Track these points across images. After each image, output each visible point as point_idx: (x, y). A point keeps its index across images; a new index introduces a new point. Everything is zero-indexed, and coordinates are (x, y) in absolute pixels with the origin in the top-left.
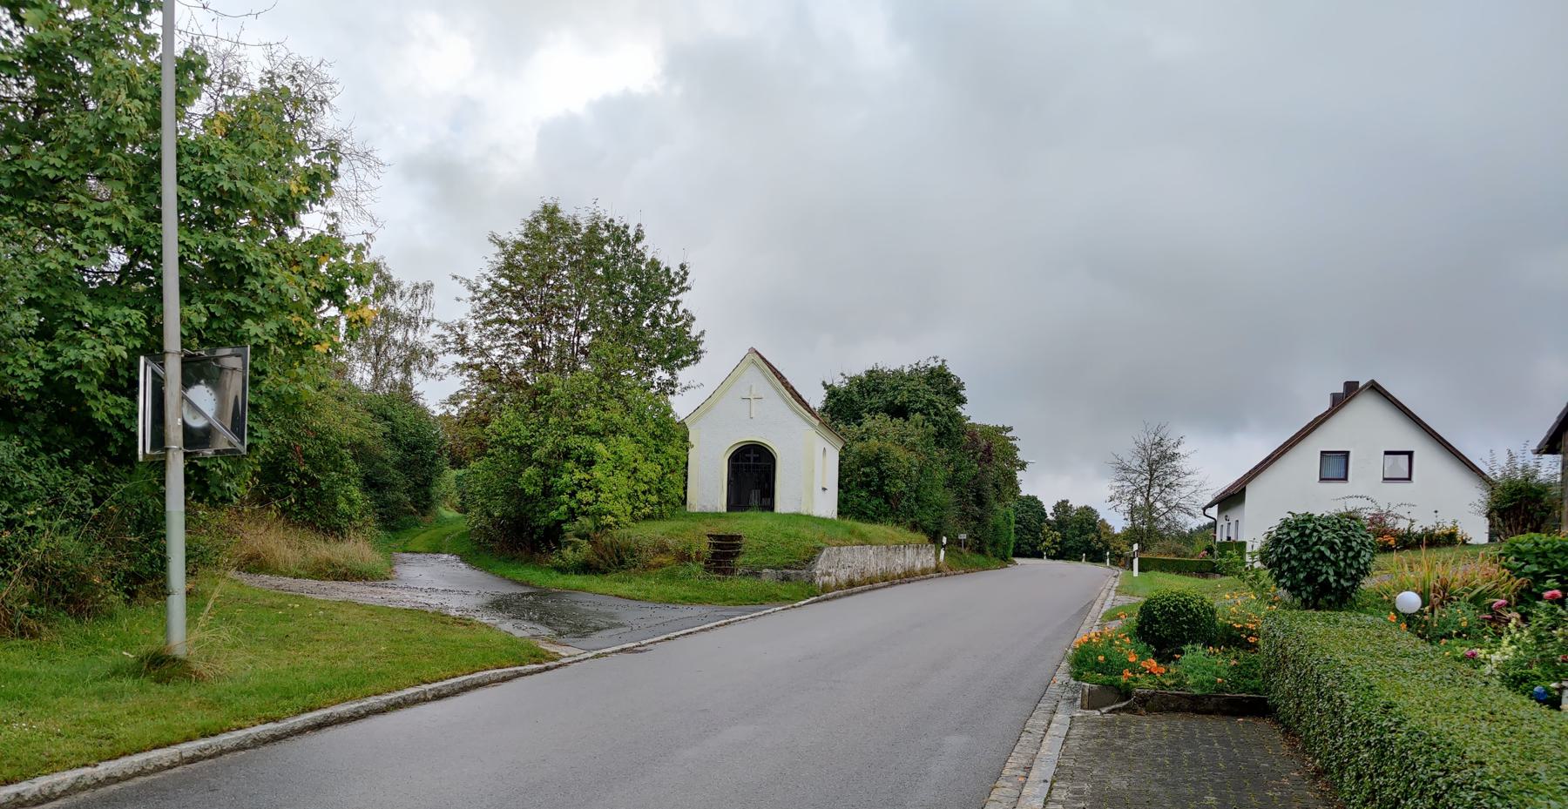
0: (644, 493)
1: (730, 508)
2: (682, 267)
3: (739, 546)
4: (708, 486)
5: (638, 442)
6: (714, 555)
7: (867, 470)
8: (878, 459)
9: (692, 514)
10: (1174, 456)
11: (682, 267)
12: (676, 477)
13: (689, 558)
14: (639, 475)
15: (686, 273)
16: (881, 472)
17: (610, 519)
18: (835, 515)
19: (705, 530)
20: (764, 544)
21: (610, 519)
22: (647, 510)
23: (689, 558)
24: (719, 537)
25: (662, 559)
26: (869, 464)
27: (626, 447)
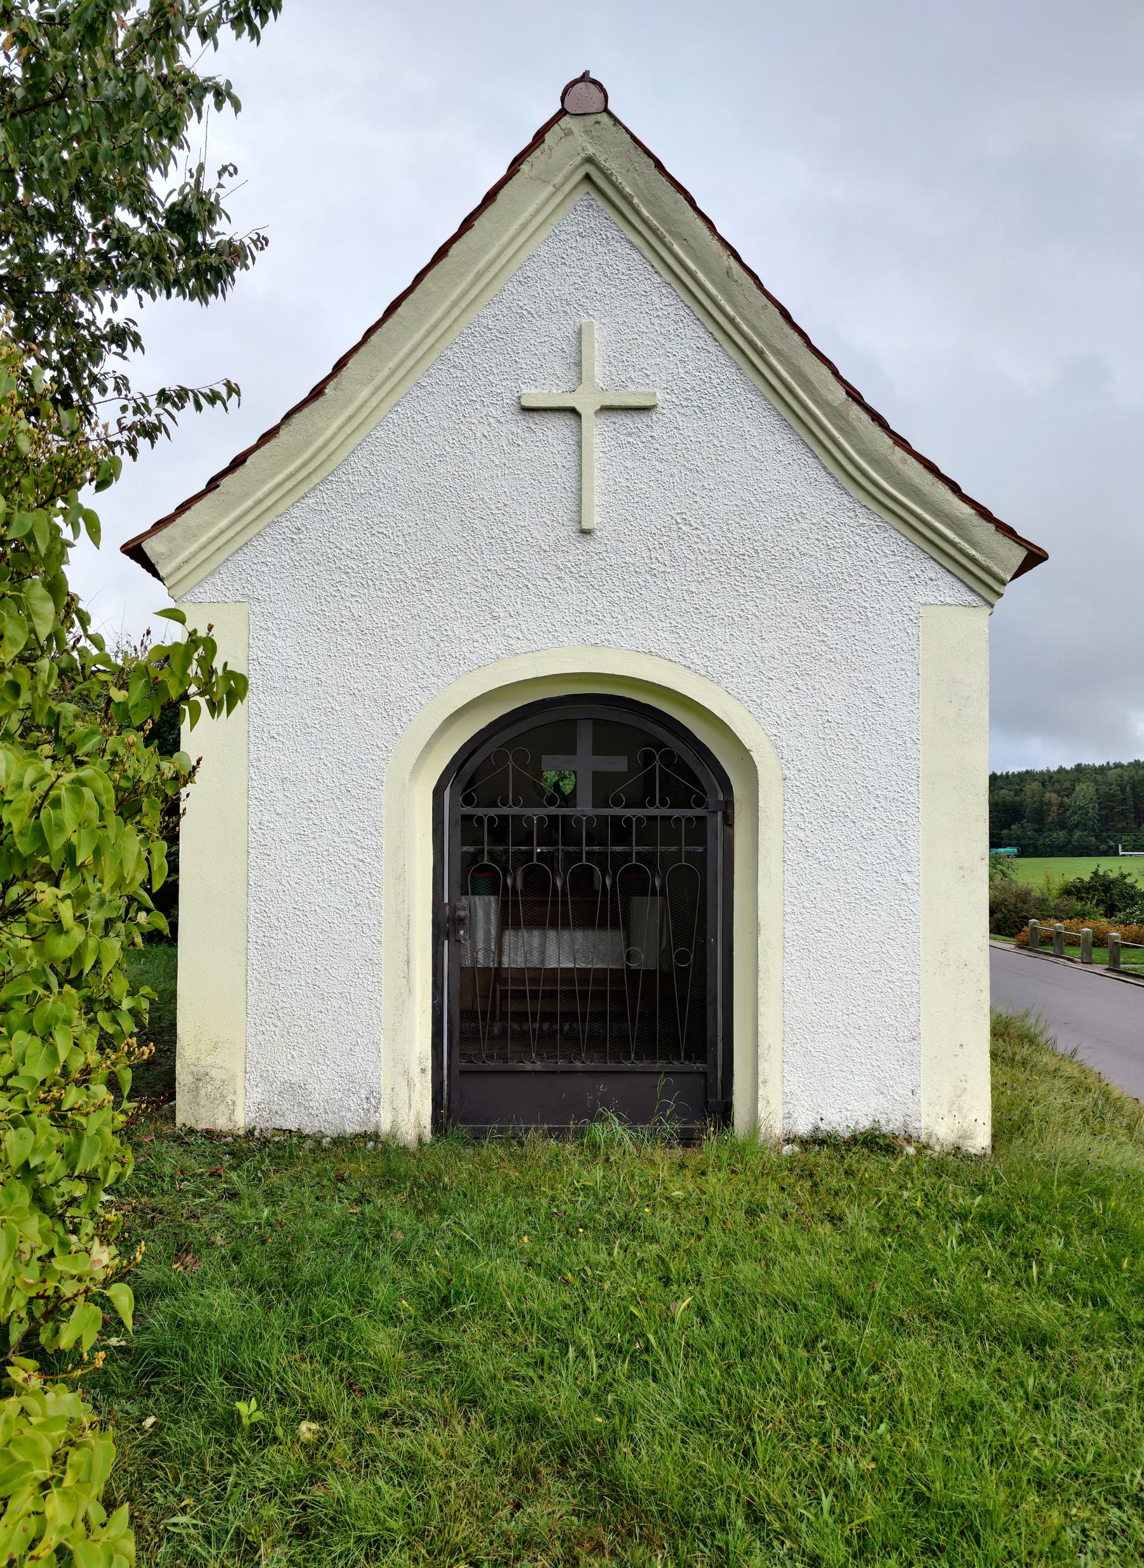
18: (406, 1106)
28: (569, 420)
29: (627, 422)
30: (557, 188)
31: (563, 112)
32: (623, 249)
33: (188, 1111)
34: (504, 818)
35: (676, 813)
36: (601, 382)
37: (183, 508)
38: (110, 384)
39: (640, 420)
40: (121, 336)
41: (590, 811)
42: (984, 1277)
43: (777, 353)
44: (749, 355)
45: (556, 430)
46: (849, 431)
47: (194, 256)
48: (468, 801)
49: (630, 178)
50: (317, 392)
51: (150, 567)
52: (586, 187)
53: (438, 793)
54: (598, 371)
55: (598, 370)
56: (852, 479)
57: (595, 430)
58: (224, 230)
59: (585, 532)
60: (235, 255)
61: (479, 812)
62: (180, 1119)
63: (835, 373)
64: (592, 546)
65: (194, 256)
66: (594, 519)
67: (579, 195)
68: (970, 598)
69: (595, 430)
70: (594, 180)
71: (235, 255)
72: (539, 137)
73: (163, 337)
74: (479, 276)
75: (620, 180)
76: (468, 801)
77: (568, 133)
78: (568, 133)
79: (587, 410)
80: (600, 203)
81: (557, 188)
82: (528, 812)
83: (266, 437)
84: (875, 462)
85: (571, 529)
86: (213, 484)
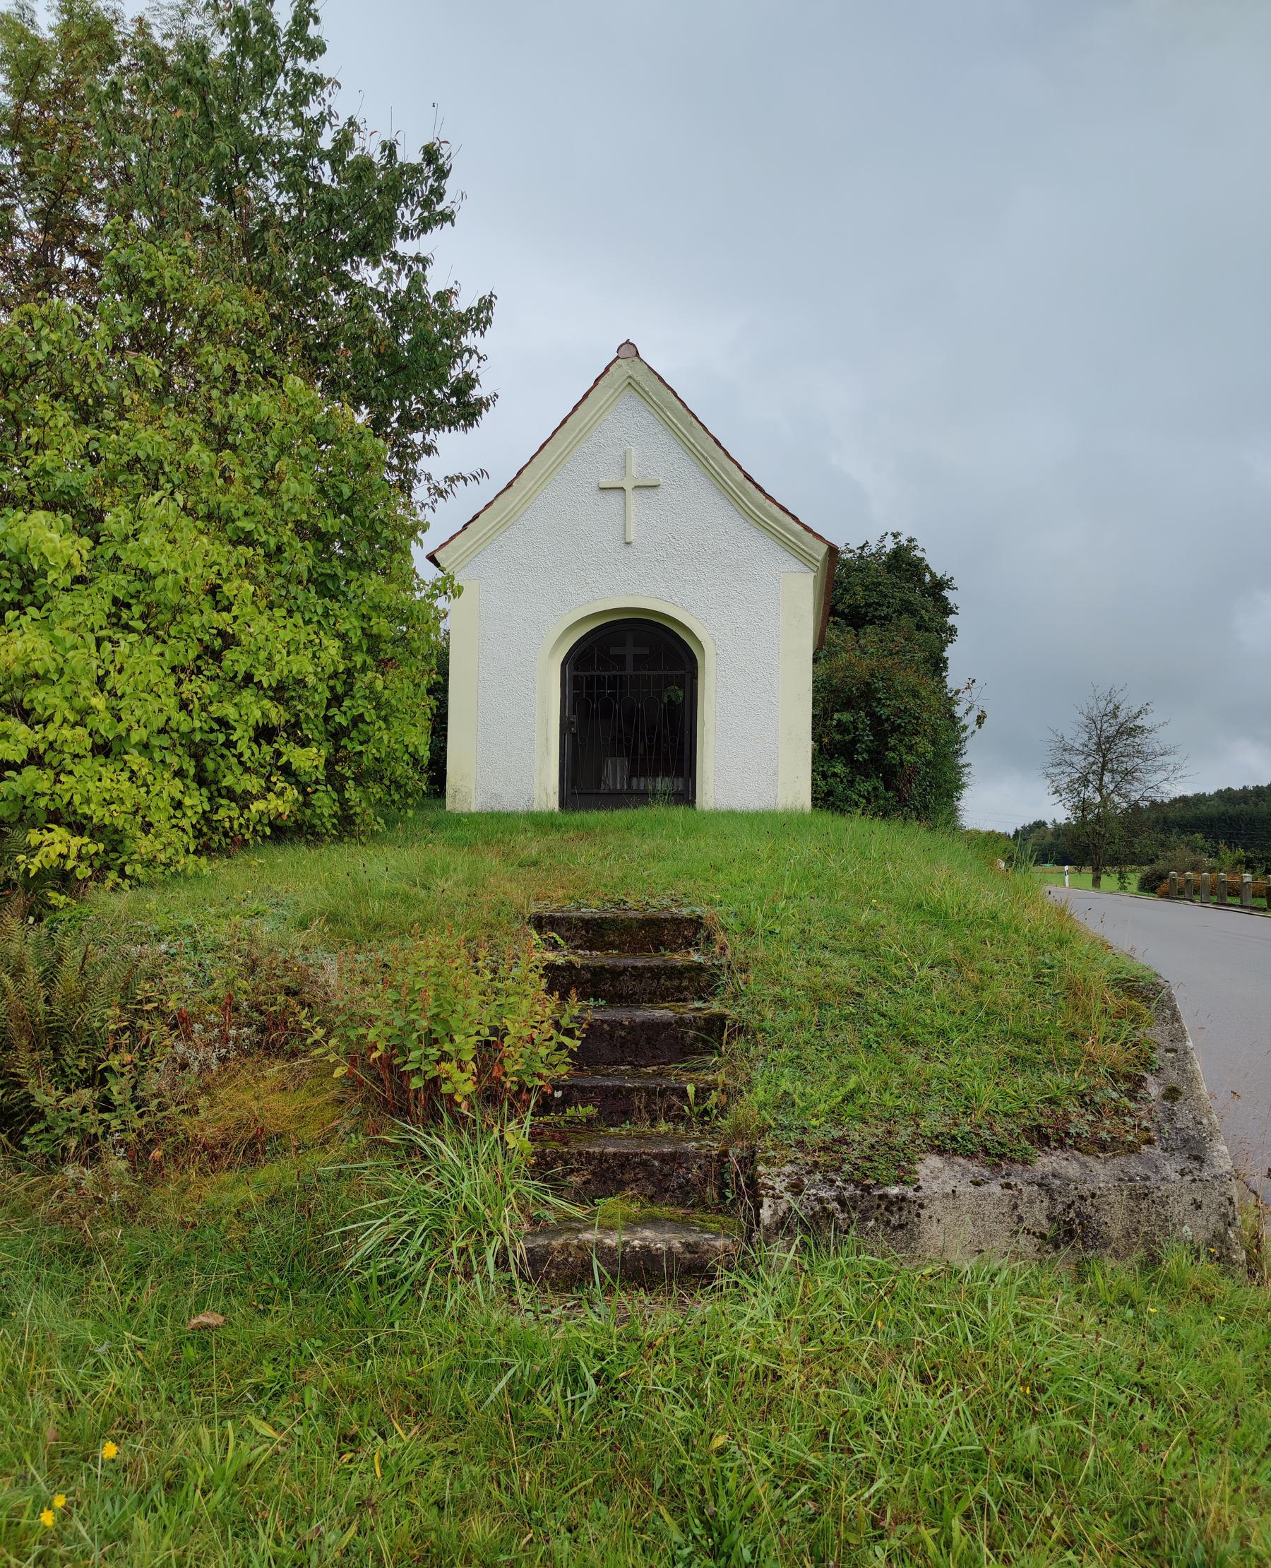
0: (264, 733)
1: (566, 801)
2: (431, 154)
3: (700, 982)
4: (508, 743)
5: (247, 540)
6: (597, 1047)
7: (846, 717)
8: (868, 693)
9: (459, 820)
10: (1133, 732)
11: (431, 154)
12: (400, 687)
13: (434, 1105)
14: (236, 661)
15: (442, 174)
16: (876, 720)
17: (57, 844)
18: (554, 803)
19: (522, 894)
20: (842, 970)
21: (57, 844)
22: (281, 804)
23: (434, 1105)
24: (592, 932)
25: (263, 1094)
26: (848, 705)
27: (174, 549)
28: (620, 492)
29: (646, 492)
30: (616, 390)
31: (618, 358)
32: (646, 414)
33: (453, 803)
34: (592, 676)
35: (671, 673)
36: (636, 474)
37: (452, 538)
38: (423, 477)
39: (655, 490)
40: (429, 449)
41: (633, 673)
42: (728, 1201)
43: (713, 459)
44: (701, 460)
45: (614, 498)
46: (746, 493)
47: (465, 409)
48: (576, 669)
49: (650, 384)
50: (510, 485)
51: (437, 565)
52: (629, 390)
53: (563, 665)
54: (634, 469)
55: (634, 470)
56: (749, 516)
57: (632, 497)
58: (477, 393)
59: (628, 543)
60: (483, 404)
61: (581, 674)
62: (448, 808)
63: (740, 467)
64: (630, 550)
65: (465, 409)
66: (632, 537)
67: (626, 391)
68: (805, 568)
69: (632, 497)
70: (631, 384)
71: (483, 404)
72: (607, 369)
73: (450, 450)
74: (581, 430)
75: (643, 385)
76: (576, 669)
77: (620, 366)
78: (620, 366)
79: (628, 488)
80: (636, 395)
81: (616, 390)
82: (603, 673)
83: (488, 506)
84: (758, 507)
85: (621, 543)
86: (465, 527)
